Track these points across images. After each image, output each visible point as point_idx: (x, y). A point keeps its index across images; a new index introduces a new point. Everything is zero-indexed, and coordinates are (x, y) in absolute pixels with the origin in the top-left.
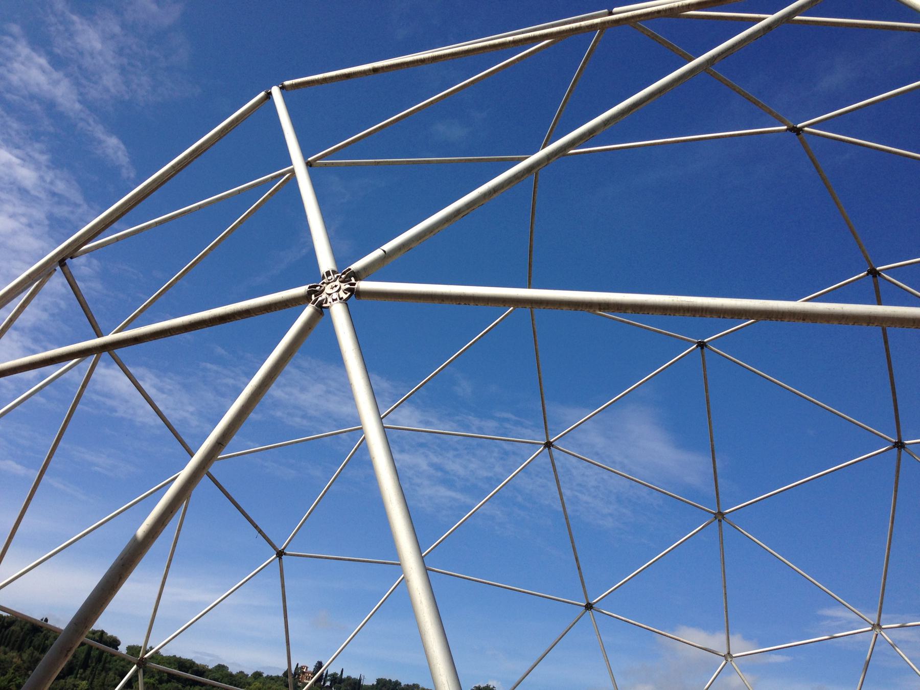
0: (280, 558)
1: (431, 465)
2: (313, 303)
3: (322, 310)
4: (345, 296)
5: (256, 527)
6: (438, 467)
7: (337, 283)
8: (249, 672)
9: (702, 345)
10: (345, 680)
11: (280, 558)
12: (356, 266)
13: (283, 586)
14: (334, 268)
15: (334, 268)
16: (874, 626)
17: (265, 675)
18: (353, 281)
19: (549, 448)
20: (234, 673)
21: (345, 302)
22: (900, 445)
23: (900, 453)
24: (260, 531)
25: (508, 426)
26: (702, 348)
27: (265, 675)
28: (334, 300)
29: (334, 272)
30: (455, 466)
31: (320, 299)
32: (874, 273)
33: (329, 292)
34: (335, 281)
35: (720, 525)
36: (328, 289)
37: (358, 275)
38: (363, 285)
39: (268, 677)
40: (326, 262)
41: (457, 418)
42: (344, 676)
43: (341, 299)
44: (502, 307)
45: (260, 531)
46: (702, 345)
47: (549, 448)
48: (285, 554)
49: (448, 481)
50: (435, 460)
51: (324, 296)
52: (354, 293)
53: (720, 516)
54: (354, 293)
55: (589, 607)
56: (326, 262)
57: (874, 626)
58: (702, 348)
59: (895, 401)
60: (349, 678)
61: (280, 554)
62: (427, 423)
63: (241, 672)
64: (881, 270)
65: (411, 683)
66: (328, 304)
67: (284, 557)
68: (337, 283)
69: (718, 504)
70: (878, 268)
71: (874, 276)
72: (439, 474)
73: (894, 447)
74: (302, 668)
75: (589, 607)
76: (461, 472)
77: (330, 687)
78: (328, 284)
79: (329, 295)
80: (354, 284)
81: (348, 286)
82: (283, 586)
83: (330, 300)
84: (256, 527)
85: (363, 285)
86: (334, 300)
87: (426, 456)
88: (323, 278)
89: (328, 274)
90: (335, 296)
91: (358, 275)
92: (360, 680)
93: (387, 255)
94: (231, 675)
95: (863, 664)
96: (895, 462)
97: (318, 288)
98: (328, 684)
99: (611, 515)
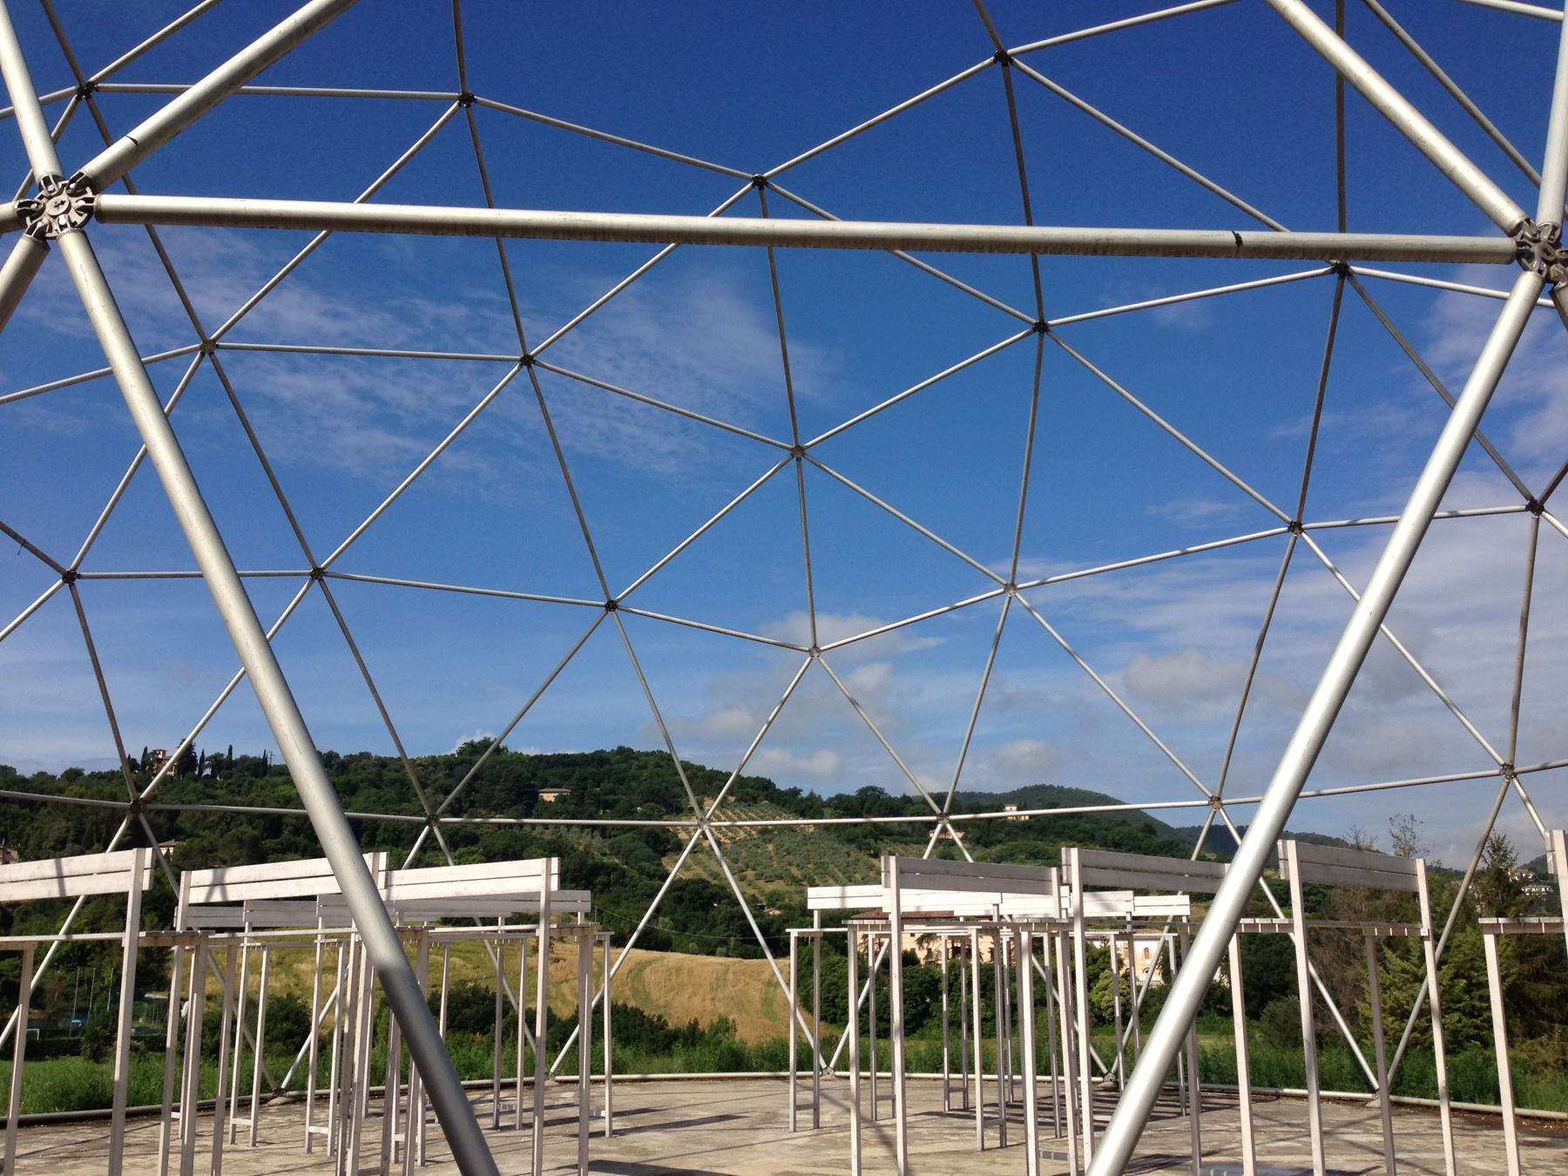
0: (72, 585)
1: (353, 391)
2: (30, 233)
3: (43, 243)
4: (79, 220)
5: (15, 536)
6: (365, 395)
7: (64, 197)
8: (57, 771)
9: (760, 183)
10: (236, 762)
11: (72, 585)
12: (92, 167)
13: (85, 629)
14: (58, 172)
15: (58, 172)
16: (1007, 587)
17: (87, 773)
18: (90, 194)
19: (529, 367)
20: (28, 775)
21: (79, 229)
22: (1041, 327)
23: (1041, 338)
24: (24, 543)
25: (488, 313)
26: (761, 188)
27: (87, 773)
28: (62, 227)
29: (57, 178)
30: (399, 392)
31: (40, 225)
32: (1004, 59)
33: (54, 213)
34: (59, 193)
35: (799, 466)
36: (50, 209)
37: (96, 184)
38: (108, 201)
39: (93, 775)
40: (42, 162)
41: (396, 303)
42: (235, 756)
43: (73, 224)
44: (308, 233)
45: (24, 543)
46: (760, 183)
47: (529, 367)
48: (79, 577)
49: (386, 417)
50: (359, 381)
51: (45, 220)
52: (89, 211)
53: (799, 452)
54: (89, 211)
55: (611, 606)
56: (42, 162)
57: (1007, 587)
58: (761, 188)
59: (284, 504)
60: (244, 759)
61: (70, 578)
62: (336, 315)
63: (42, 774)
64: (1015, 54)
65: (356, 752)
66: (54, 234)
67: (77, 582)
68: (64, 197)
69: (795, 433)
70: (1010, 51)
71: (1005, 65)
72: (370, 407)
73: (1034, 330)
74: (155, 753)
75: (611, 606)
76: (410, 400)
77: (213, 776)
78: (50, 198)
79: (55, 217)
80: (91, 200)
81: (82, 203)
82: (85, 629)
83: (56, 227)
84: (15, 536)
85: (108, 201)
86: (62, 227)
87: (343, 377)
88: (41, 188)
89: (47, 181)
90: (63, 220)
91: (96, 184)
92: (265, 759)
93: (139, 148)
94: (23, 780)
95: (993, 638)
96: (1035, 353)
97: (34, 206)
98: (208, 771)
99: (673, 453)
